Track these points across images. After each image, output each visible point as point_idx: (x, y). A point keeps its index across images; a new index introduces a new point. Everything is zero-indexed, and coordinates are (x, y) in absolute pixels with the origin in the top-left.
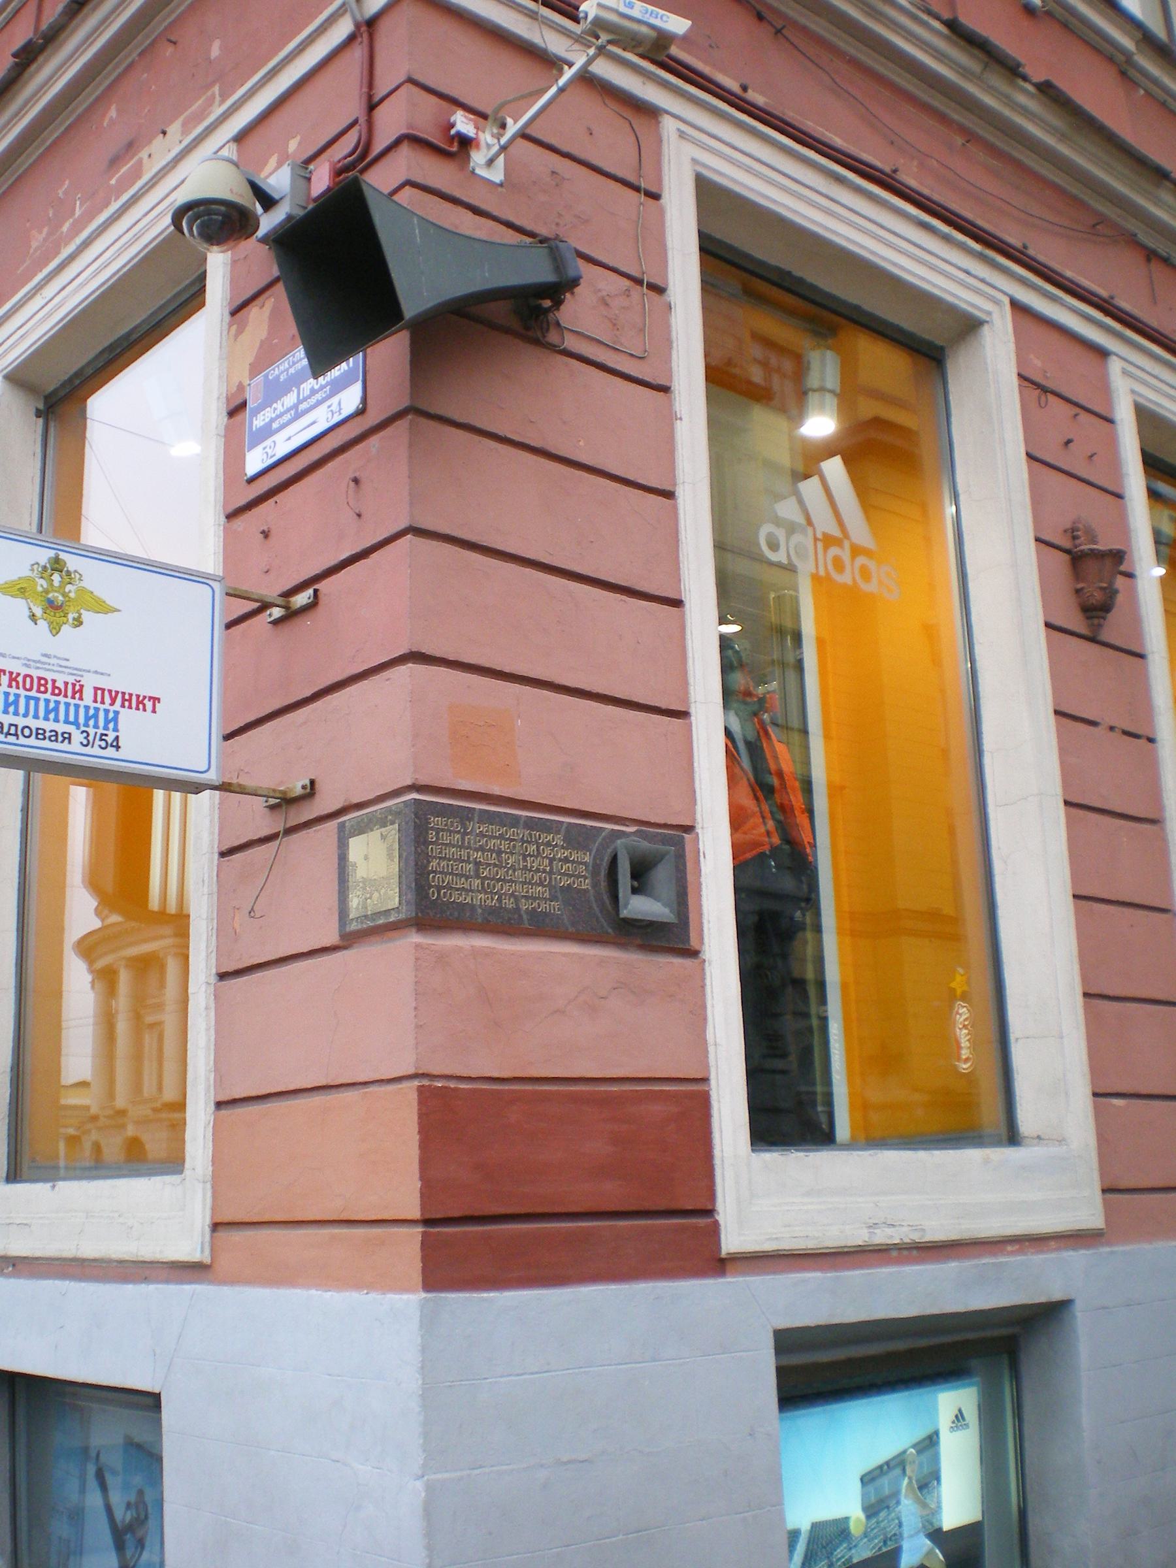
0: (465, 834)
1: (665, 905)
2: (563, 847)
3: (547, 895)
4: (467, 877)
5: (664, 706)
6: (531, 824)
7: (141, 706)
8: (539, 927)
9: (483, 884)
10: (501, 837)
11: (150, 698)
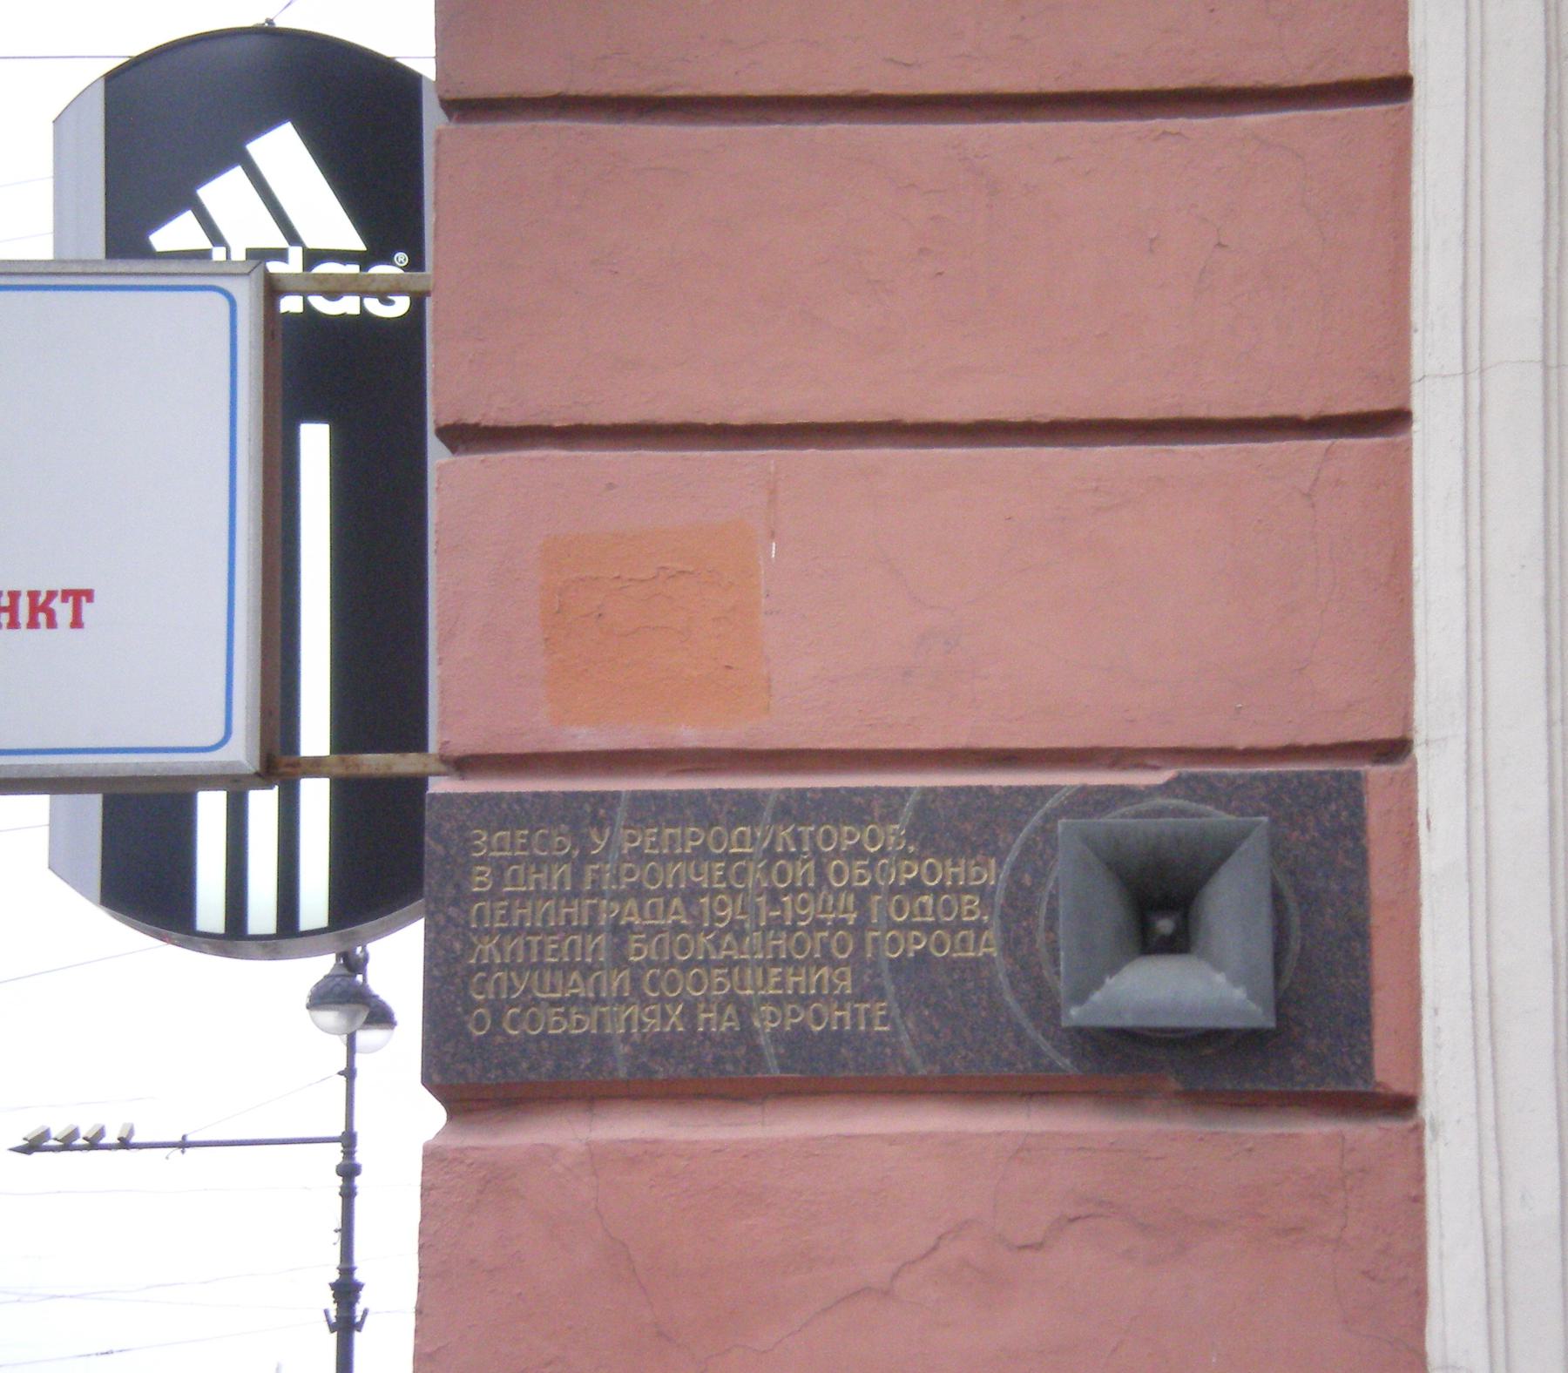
0: (585, 858)
1: (1235, 981)
2: (905, 854)
3: (847, 986)
4: (586, 970)
5: (1307, 408)
6: (793, 808)
7: (42, 617)
8: (821, 1071)
9: (636, 980)
10: (702, 853)
11: (66, 594)
